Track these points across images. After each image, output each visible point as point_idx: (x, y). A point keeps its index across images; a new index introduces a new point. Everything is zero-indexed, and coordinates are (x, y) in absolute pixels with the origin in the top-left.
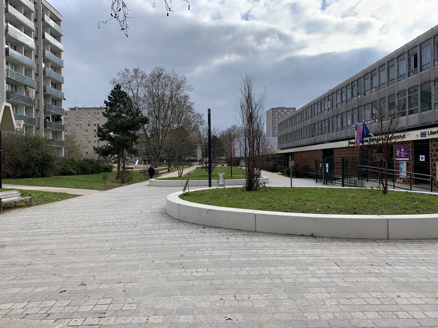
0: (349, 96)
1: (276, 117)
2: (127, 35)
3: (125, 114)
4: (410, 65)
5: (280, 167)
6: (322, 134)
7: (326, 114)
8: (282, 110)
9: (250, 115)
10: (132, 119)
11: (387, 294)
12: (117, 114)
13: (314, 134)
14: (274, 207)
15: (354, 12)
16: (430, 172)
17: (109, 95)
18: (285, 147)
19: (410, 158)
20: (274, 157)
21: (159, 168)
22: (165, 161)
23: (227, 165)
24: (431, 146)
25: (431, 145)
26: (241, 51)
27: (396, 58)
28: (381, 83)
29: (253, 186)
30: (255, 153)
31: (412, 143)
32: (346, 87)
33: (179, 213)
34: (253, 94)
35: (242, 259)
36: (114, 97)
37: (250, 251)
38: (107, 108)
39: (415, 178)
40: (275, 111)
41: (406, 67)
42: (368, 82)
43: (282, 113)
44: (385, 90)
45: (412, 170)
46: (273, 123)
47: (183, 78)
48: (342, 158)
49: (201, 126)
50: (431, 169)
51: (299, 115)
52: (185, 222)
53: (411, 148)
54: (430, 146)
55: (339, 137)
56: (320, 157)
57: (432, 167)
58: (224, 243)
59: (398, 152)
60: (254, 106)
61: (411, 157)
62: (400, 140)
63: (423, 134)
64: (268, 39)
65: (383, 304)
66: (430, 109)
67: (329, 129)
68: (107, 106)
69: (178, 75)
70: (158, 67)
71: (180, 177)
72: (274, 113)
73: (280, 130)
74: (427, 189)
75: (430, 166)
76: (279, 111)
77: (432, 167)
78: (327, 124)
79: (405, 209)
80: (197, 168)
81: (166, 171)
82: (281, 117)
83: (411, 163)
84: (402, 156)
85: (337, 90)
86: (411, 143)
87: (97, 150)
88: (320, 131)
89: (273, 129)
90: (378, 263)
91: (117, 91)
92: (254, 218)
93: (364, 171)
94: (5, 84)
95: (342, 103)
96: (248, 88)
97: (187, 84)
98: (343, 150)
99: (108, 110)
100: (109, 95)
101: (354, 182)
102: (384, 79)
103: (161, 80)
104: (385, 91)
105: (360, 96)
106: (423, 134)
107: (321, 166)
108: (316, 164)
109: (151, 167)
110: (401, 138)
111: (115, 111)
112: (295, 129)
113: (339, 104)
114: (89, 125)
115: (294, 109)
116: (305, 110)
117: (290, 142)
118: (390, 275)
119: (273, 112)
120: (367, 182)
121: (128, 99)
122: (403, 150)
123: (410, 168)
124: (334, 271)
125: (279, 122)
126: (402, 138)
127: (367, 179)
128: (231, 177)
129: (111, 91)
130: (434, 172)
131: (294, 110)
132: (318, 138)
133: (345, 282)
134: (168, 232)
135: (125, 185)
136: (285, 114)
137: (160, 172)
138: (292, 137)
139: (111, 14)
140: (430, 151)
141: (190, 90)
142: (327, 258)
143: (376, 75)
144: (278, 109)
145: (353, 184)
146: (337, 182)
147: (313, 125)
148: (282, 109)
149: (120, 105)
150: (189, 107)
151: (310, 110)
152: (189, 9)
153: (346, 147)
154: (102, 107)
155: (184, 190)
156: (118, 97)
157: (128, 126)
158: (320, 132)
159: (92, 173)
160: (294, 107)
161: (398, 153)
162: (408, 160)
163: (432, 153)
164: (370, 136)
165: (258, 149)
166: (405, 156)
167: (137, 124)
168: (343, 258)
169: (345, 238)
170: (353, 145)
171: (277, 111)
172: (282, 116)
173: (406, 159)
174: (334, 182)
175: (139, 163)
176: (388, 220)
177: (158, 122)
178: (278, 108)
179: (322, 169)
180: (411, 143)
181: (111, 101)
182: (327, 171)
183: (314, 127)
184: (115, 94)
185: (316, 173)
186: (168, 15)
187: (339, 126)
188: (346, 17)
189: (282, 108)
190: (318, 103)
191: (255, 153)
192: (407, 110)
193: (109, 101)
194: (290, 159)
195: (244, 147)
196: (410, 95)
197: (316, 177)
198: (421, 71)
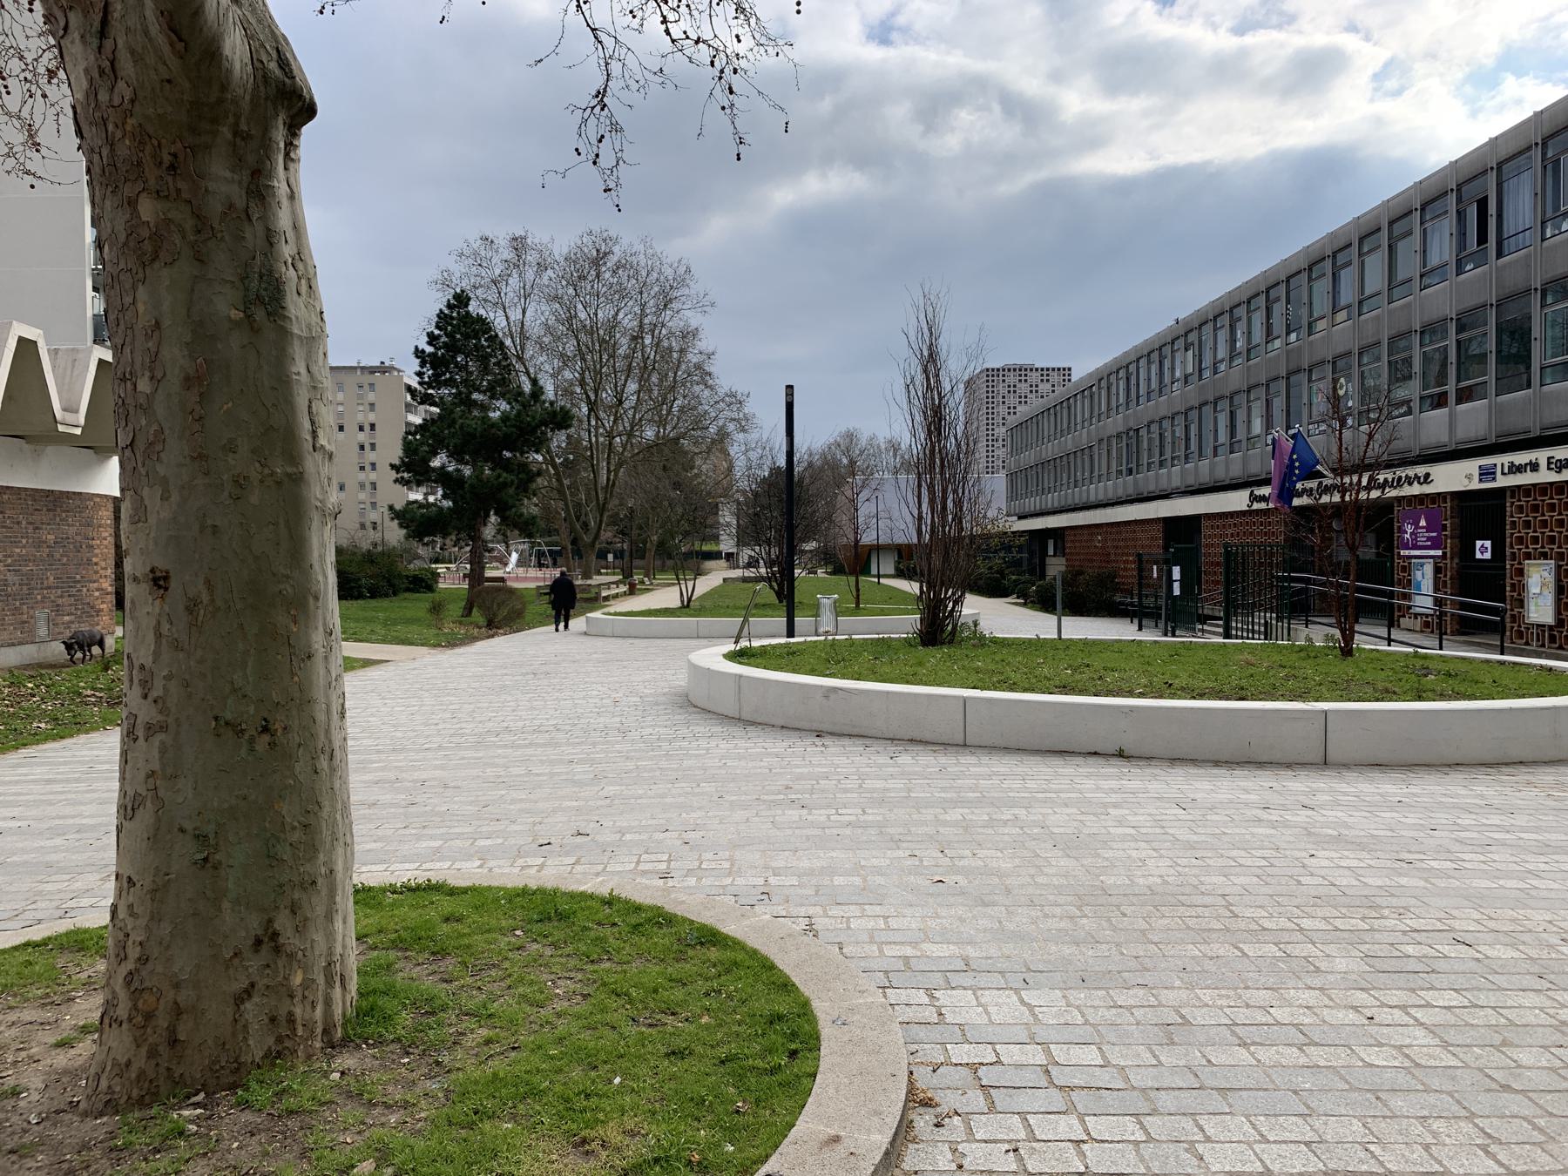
0: (1258, 335)
1: (1001, 400)
2: (617, 206)
3: (484, 392)
4: (1465, 234)
5: (1014, 577)
6: (1162, 464)
7: (1179, 397)
8: (1020, 375)
9: (936, 412)
10: (519, 412)
11: (1288, 853)
12: (460, 393)
13: (1133, 466)
14: (1014, 684)
15: (1281, 13)
16: (1507, 594)
17: (432, 328)
18: (1032, 509)
19: (1445, 548)
20: (1007, 541)
21: (597, 580)
22: (610, 557)
23: (826, 573)
24: (1512, 514)
25: (1511, 506)
26: (865, 157)
27: (1416, 209)
28: (1368, 292)
29: (943, 631)
30: (949, 532)
31: (1451, 501)
32: (1249, 302)
33: (739, 699)
34: (945, 348)
35: (943, 795)
36: (445, 334)
37: (959, 781)
38: (424, 373)
39: (1459, 615)
40: (995, 378)
41: (1451, 241)
42: (1322, 286)
43: (1023, 388)
44: (1377, 317)
45: (1451, 588)
46: (990, 421)
47: (682, 269)
48: (1226, 548)
49: (741, 436)
50: (1508, 585)
51: (1083, 397)
52: (760, 724)
53: (1448, 517)
54: (1508, 509)
55: (1221, 475)
56: (1154, 544)
57: (1512, 579)
58: (887, 766)
59: (1409, 528)
60: (947, 386)
61: (1448, 545)
62: (1416, 489)
63: (1487, 473)
64: (964, 116)
65: (1272, 865)
66: (1529, 386)
67: (1187, 448)
68: (422, 367)
69: (663, 259)
70: (596, 229)
71: (687, 607)
72: (993, 386)
73: (1015, 451)
74: (1489, 648)
75: (1505, 575)
76: (1012, 379)
77: (1512, 579)
78: (1180, 432)
79: (1387, 691)
80: (724, 580)
81: (623, 588)
82: (1018, 400)
83: (1449, 565)
84: (1421, 544)
85: (1217, 311)
86: (1448, 500)
87: (406, 516)
88: (1158, 455)
89: (990, 443)
90: (1283, 805)
91: (458, 313)
92: (962, 709)
93: (1300, 591)
94: (90, 293)
95: (1232, 359)
96: (930, 330)
97: (695, 288)
98: (1231, 521)
99: (427, 379)
100: (432, 328)
101: (1262, 629)
102: (1376, 279)
103: (607, 275)
104: (1380, 321)
105: (1293, 336)
106: (1487, 473)
107: (1155, 575)
108: (1140, 570)
109: (563, 574)
110: (1419, 483)
111: (450, 383)
112: (1070, 447)
113: (1222, 360)
114: (341, 428)
115: (1067, 372)
116: (1104, 379)
117: (1052, 490)
118: (1305, 825)
119: (990, 384)
120: (1307, 627)
121: (494, 339)
122: (1423, 523)
123: (1445, 582)
124: (1173, 818)
125: (1012, 420)
126: (1421, 484)
127: (1307, 616)
128: (857, 610)
129: (438, 316)
130: (1519, 594)
131: (1064, 375)
132: (1149, 480)
133: (1196, 833)
134: (723, 745)
135: (502, 634)
136: (1031, 391)
137: (604, 594)
138: (1059, 475)
139: (577, 150)
140: (1508, 527)
141: (705, 308)
142: (1157, 795)
143: (1349, 264)
144: (1006, 373)
145: (1259, 633)
146: (1209, 628)
147: (1131, 433)
148: (1023, 373)
149: (467, 362)
150: (698, 366)
151: (1121, 382)
152: (786, 131)
153: (1243, 513)
154: (387, 364)
155: (736, 642)
156: (462, 334)
157: (506, 435)
158: (1156, 459)
159: (372, 597)
160: (1066, 366)
161: (1409, 531)
162: (1438, 557)
163: (1512, 534)
164: (1320, 475)
165: (958, 519)
166: (1429, 543)
167: (534, 430)
168: (1198, 796)
169: (1208, 761)
170: (1263, 506)
171: (1004, 381)
172: (1020, 397)
173: (1432, 553)
174: (1200, 627)
175: (520, 563)
176: (1325, 712)
177: (593, 423)
178: (1009, 370)
179: (1161, 587)
180: (1448, 500)
181: (436, 348)
182: (1177, 591)
183: (1134, 441)
184: (451, 325)
185: (1140, 599)
186: (739, 159)
187: (1223, 437)
188: (1251, 33)
189: (1020, 370)
190: (1149, 355)
191: (949, 532)
192: (1451, 387)
193: (429, 349)
194: (1051, 552)
195: (916, 513)
196: (1463, 336)
197: (1139, 614)
198: (1500, 255)
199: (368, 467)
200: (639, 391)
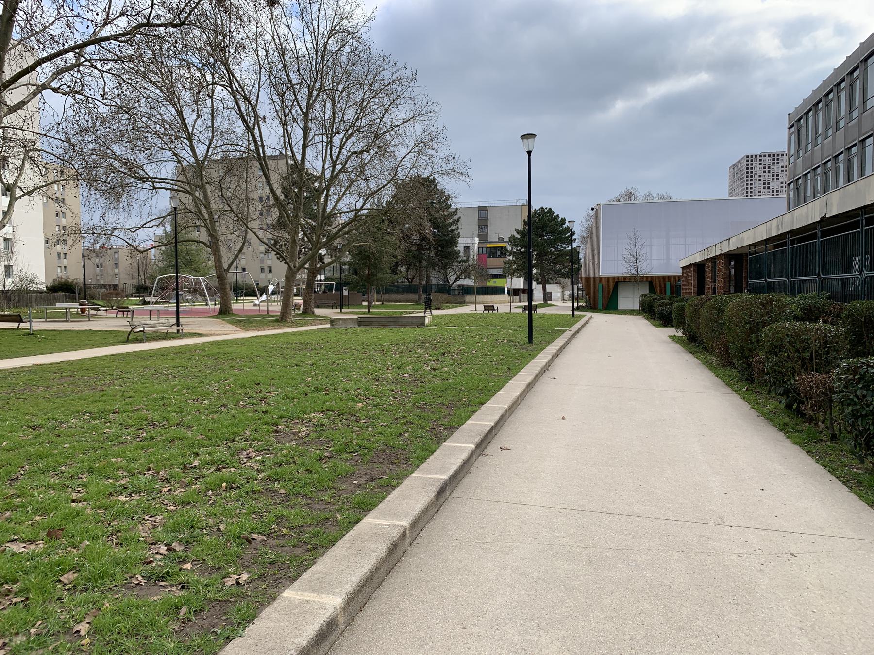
1: (758, 178)
72: (752, 168)
171: (760, 164)
178: (765, 156)
199: (267, 270)
200: (254, 108)
